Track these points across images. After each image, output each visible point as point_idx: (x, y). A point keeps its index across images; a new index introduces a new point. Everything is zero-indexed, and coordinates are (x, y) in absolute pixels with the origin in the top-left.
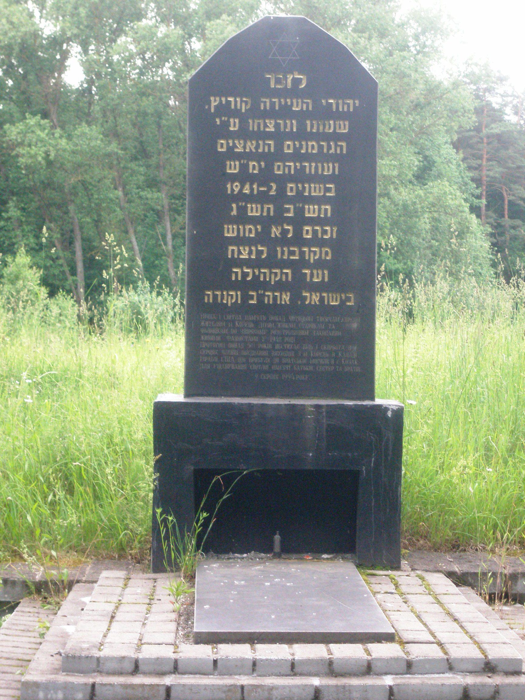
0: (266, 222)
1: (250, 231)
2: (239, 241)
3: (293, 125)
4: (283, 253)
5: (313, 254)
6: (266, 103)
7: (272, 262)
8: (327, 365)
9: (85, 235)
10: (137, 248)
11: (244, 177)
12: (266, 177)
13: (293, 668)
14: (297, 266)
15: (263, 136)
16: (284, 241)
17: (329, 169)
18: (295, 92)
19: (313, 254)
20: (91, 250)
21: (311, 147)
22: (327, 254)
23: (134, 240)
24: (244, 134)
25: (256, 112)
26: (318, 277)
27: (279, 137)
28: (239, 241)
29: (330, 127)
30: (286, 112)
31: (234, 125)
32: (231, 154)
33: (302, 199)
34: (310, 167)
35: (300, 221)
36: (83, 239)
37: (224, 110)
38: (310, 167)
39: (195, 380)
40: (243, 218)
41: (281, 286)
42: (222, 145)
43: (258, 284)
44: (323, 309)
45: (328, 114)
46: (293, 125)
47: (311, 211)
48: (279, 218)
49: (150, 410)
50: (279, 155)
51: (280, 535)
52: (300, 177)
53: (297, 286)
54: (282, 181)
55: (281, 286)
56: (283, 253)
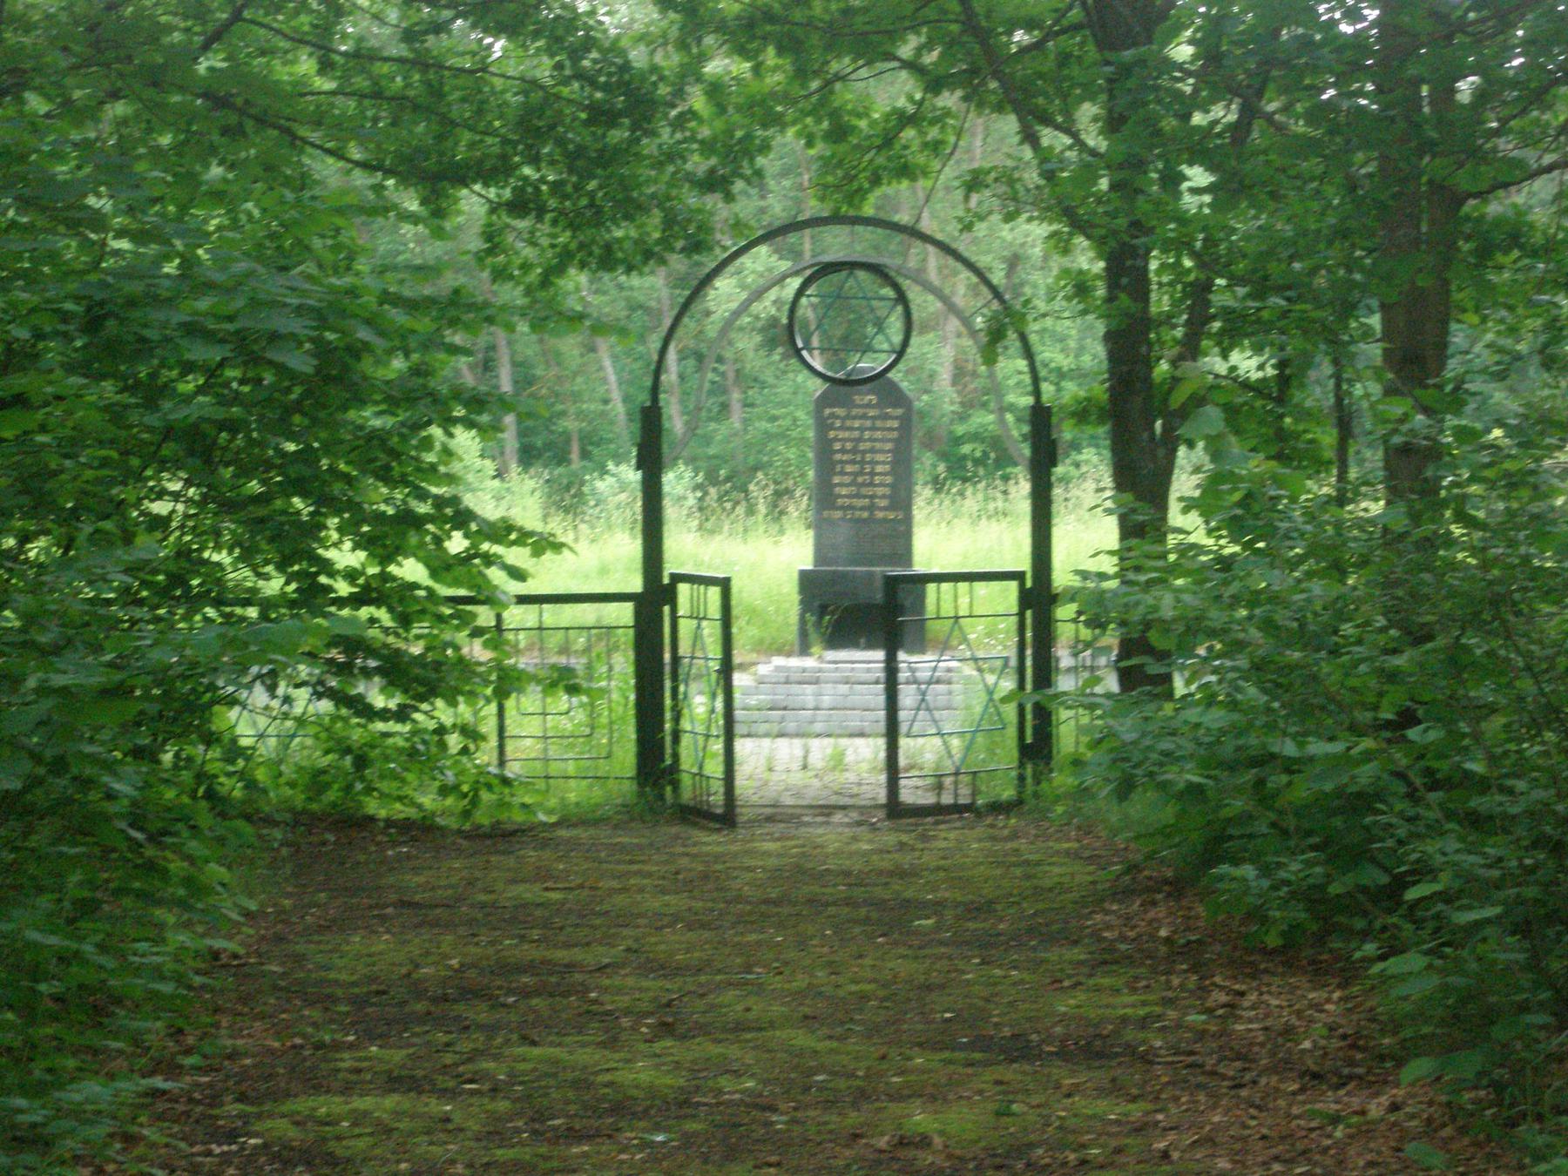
0: (856, 474)
1: (847, 479)
2: (841, 485)
3: (868, 423)
4: (864, 491)
5: (880, 491)
6: (854, 412)
7: (857, 496)
8: (956, 783)
9: (519, 359)
10: (613, 378)
11: (843, 451)
12: (854, 451)
13: (868, 670)
14: (872, 497)
15: (851, 429)
16: (863, 484)
17: (889, 446)
18: (869, 405)
19: (880, 491)
20: (530, 384)
21: (878, 435)
22: (887, 491)
23: (607, 363)
24: (842, 428)
25: (848, 417)
26: (883, 503)
27: (862, 429)
28: (841, 485)
29: (889, 423)
30: (864, 417)
31: (838, 424)
32: (836, 439)
33: (874, 463)
34: (878, 445)
35: (873, 474)
36: (514, 364)
37: (833, 416)
38: (878, 445)
39: (820, 557)
40: (843, 473)
41: (862, 509)
42: (832, 434)
43: (851, 507)
44: (885, 520)
45: (886, 417)
46: (868, 423)
47: (879, 469)
48: (861, 473)
49: (796, 576)
50: (860, 440)
51: (1191, 164)
52: (873, 451)
53: (871, 508)
54: (864, 452)
55: (862, 509)
56: (864, 491)
